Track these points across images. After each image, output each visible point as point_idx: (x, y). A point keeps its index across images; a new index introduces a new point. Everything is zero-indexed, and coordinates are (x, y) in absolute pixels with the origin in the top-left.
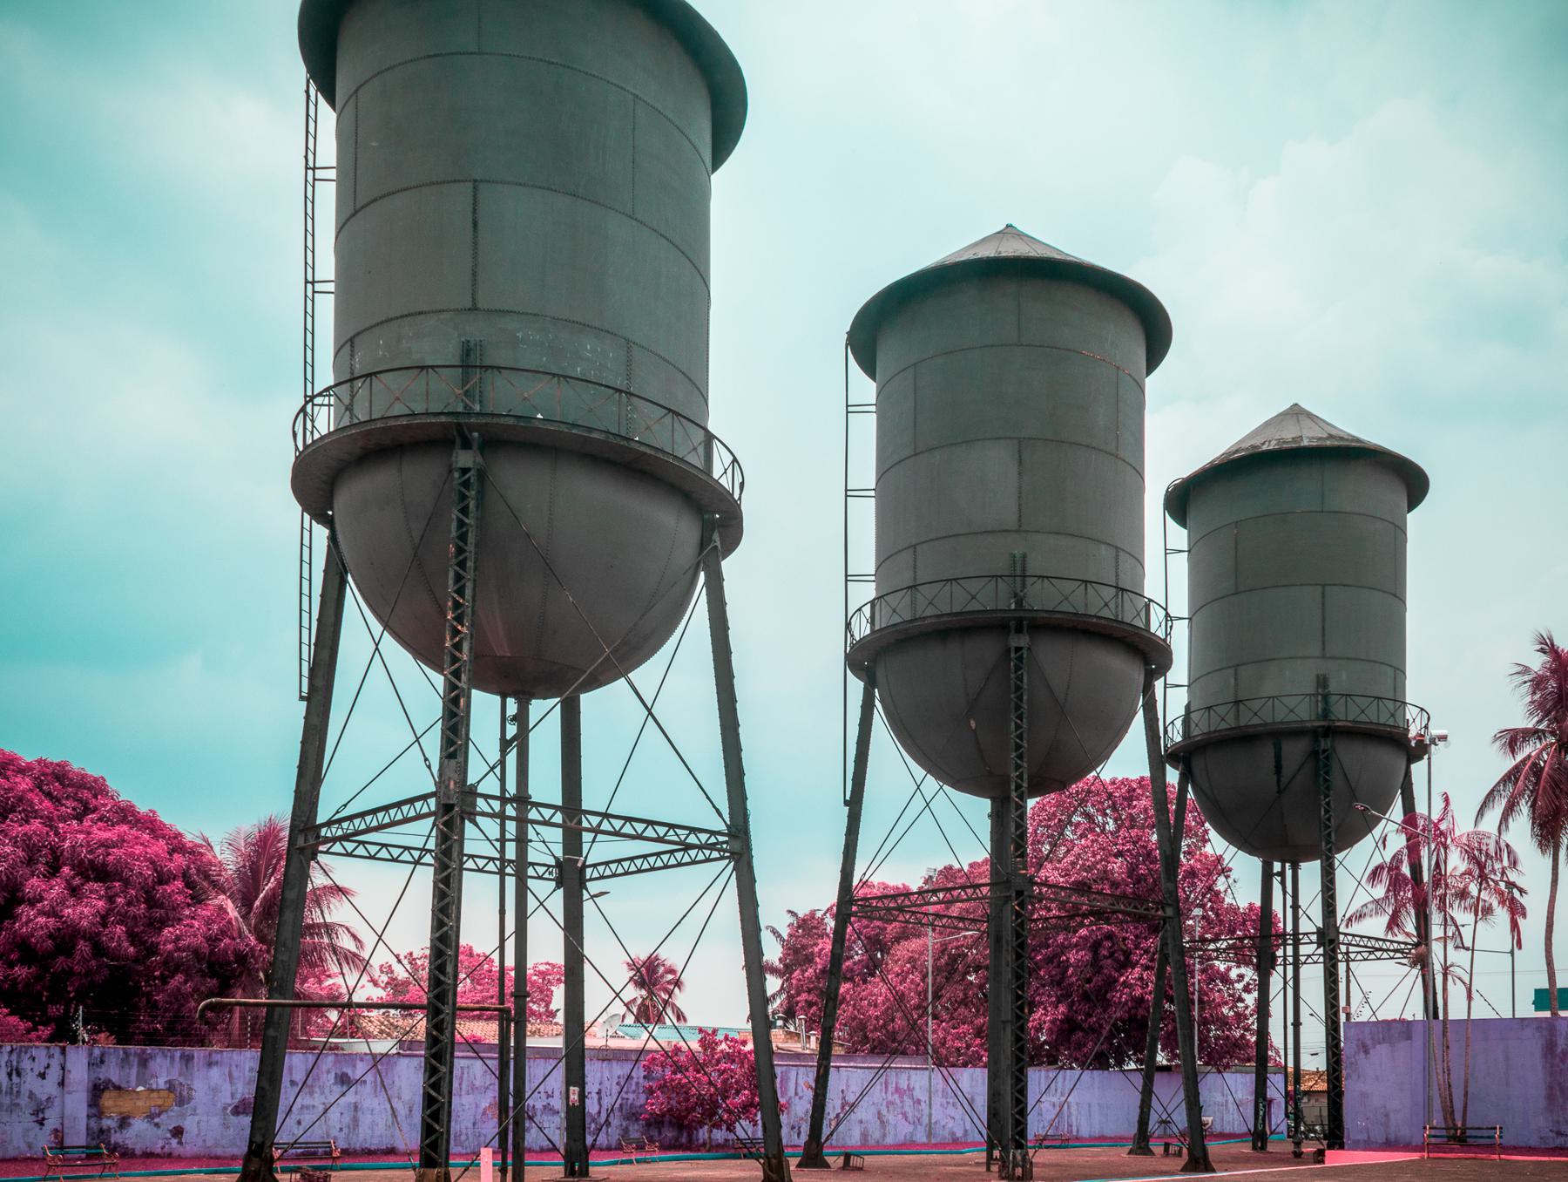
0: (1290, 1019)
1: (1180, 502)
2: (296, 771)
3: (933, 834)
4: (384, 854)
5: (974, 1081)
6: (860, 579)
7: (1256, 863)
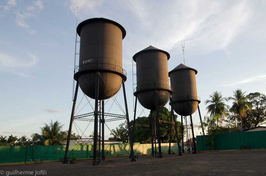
0: (186, 121)
1: (170, 73)
2: (71, 113)
3: (144, 112)
4: (86, 120)
5: (151, 144)
6: (135, 84)
7: (180, 116)
